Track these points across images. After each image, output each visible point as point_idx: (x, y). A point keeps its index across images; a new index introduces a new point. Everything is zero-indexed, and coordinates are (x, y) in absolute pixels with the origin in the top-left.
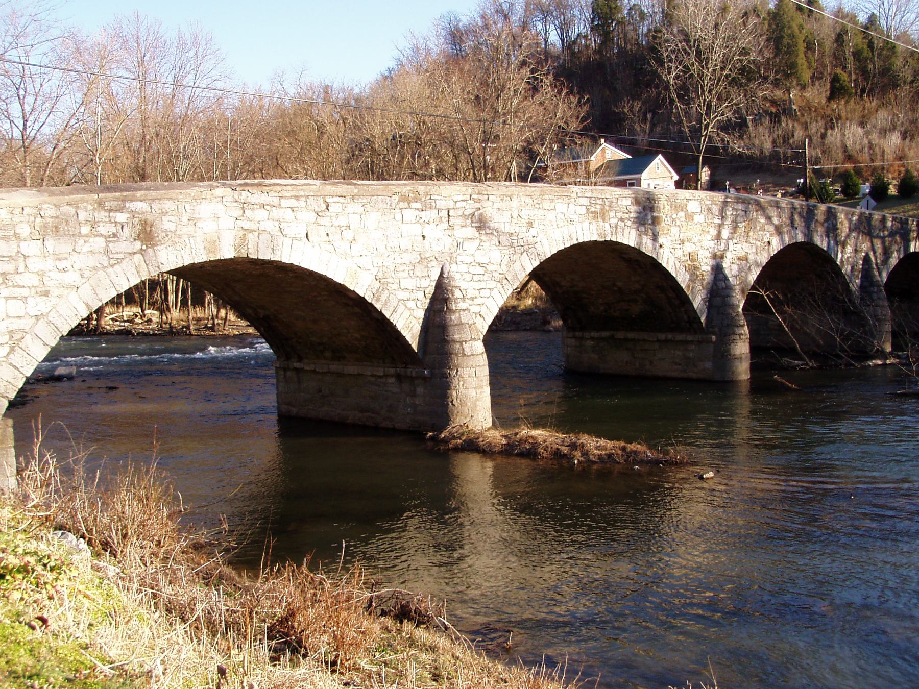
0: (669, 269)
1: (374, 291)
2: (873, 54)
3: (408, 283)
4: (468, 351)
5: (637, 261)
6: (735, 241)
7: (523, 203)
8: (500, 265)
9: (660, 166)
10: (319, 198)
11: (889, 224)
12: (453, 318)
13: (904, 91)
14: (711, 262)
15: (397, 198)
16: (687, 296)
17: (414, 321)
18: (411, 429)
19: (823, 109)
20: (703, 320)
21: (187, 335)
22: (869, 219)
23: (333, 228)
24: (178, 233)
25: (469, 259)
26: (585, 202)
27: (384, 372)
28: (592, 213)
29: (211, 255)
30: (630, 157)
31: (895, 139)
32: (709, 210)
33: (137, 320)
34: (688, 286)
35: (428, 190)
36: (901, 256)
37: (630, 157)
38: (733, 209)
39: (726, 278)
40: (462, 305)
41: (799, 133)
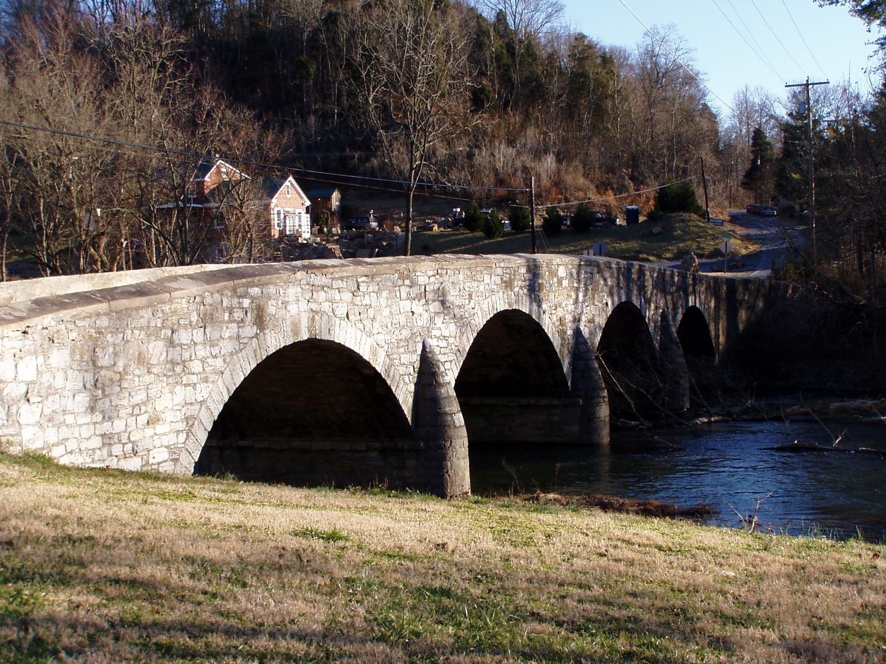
3: (405, 359)
9: (291, 190)
12: (443, 391)
31: (549, 162)
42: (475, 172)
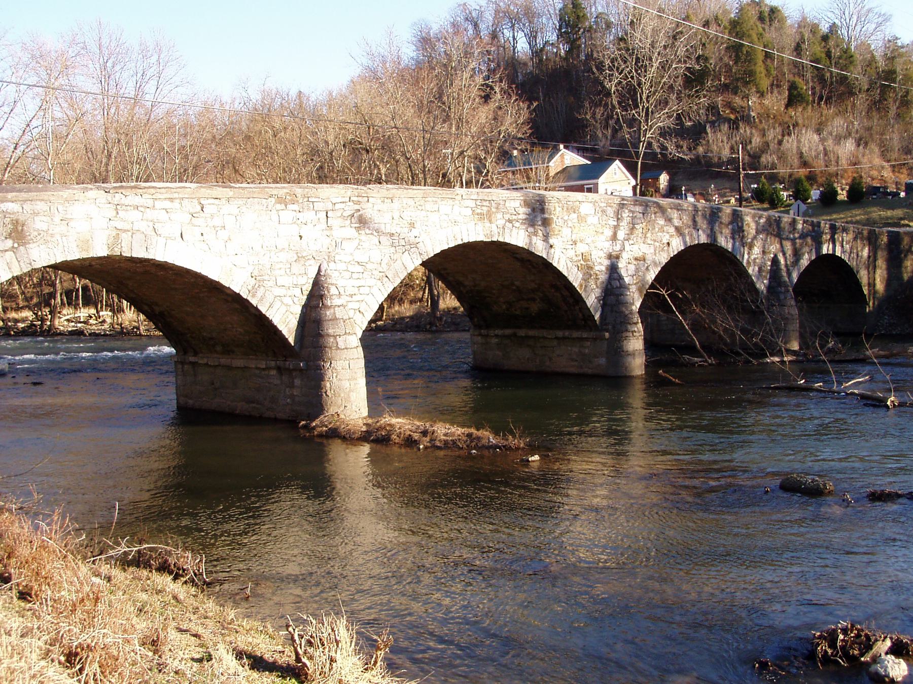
0: (560, 269)
1: (250, 288)
2: (831, 63)
4: (341, 345)
5: (529, 261)
6: (631, 242)
7: (404, 205)
8: (380, 264)
9: (618, 171)
10: (194, 200)
11: (800, 226)
12: (328, 313)
13: (861, 101)
14: (607, 262)
15: (273, 200)
16: (580, 295)
17: (291, 316)
18: (290, 418)
19: (781, 116)
20: (597, 317)
21: (137, 335)
22: (778, 222)
23: (208, 228)
24: (50, 232)
25: (348, 258)
26: (472, 204)
27: (266, 364)
28: (478, 214)
29: (84, 252)
30: (589, 163)
31: (849, 146)
32: (603, 211)
33: (92, 321)
34: (581, 286)
35: (305, 193)
36: (813, 258)
37: (589, 163)
38: (630, 211)
39: (620, 278)
40: (336, 301)
41: (756, 141)
42: (782, 157)
